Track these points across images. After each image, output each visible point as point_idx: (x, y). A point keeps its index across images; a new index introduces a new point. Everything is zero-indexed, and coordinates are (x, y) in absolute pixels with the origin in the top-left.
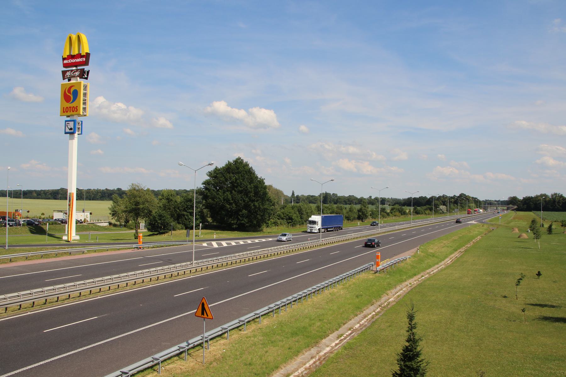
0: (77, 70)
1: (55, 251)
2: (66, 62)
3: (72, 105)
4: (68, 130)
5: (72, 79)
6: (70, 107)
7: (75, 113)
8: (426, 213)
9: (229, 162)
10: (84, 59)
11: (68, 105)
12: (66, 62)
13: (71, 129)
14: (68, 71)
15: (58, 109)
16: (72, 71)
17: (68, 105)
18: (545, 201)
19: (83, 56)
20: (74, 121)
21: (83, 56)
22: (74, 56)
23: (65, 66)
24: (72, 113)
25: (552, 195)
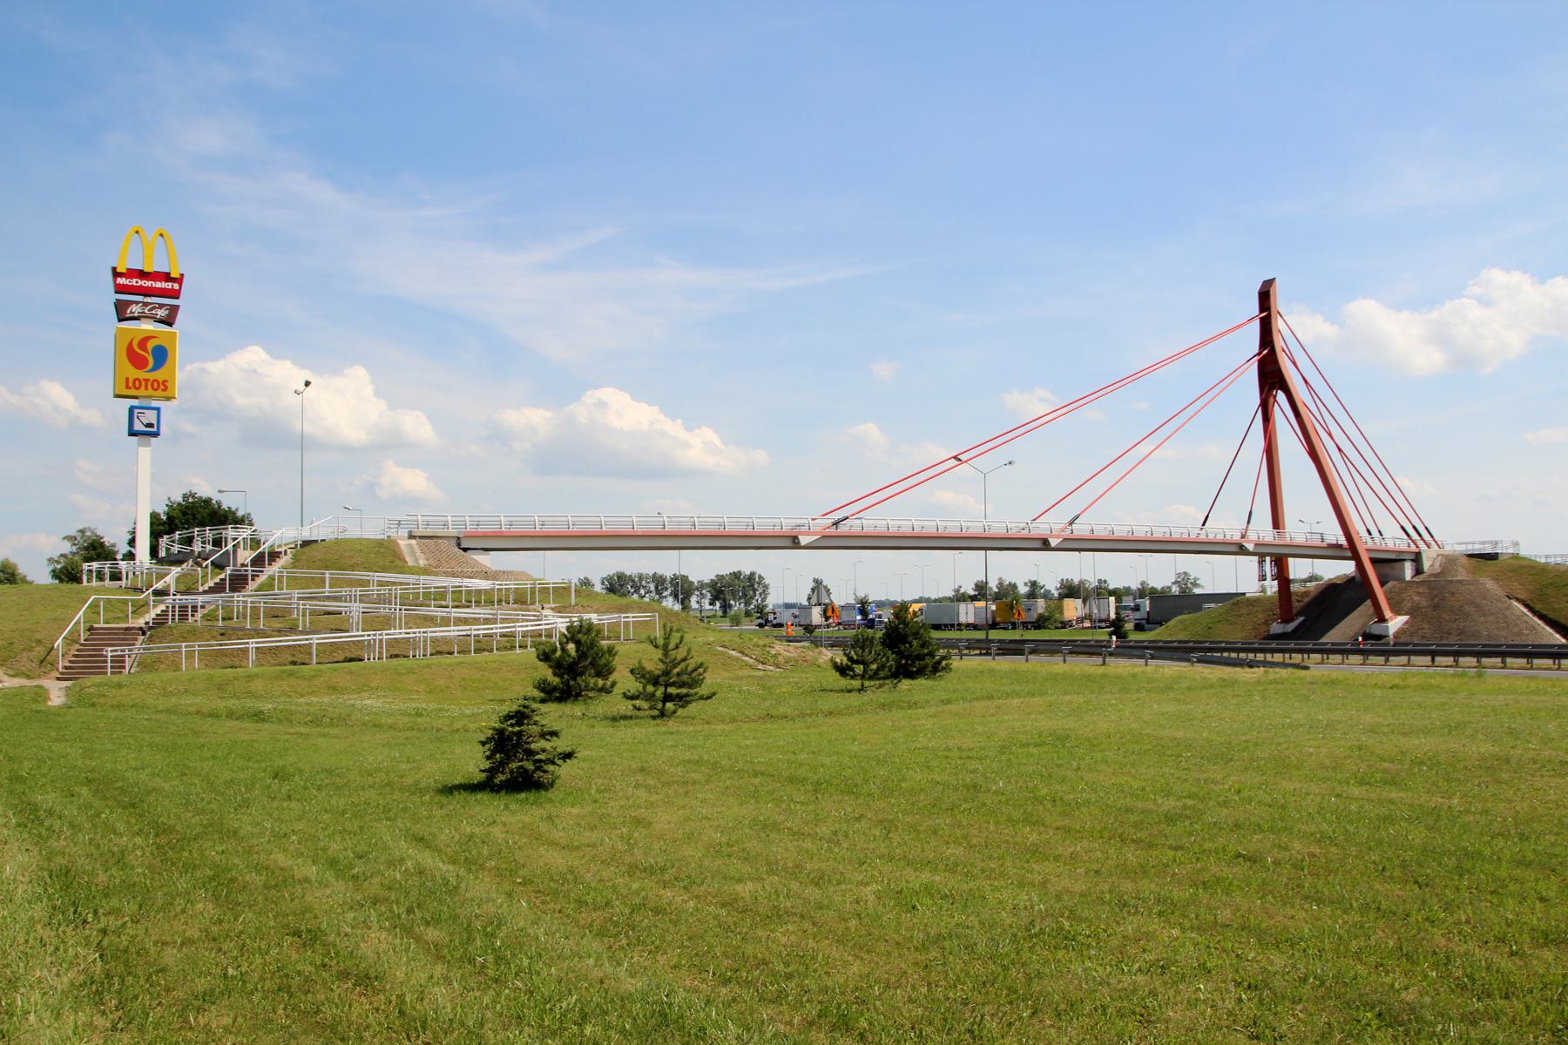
0: (161, 306)
2: (121, 281)
3: (152, 376)
4: (138, 427)
6: (146, 381)
7: (160, 393)
10: (176, 286)
11: (141, 374)
12: (121, 281)
13: (150, 425)
16: (146, 304)
19: (174, 280)
20: (158, 409)
21: (174, 280)
23: (120, 289)
24: (150, 392)
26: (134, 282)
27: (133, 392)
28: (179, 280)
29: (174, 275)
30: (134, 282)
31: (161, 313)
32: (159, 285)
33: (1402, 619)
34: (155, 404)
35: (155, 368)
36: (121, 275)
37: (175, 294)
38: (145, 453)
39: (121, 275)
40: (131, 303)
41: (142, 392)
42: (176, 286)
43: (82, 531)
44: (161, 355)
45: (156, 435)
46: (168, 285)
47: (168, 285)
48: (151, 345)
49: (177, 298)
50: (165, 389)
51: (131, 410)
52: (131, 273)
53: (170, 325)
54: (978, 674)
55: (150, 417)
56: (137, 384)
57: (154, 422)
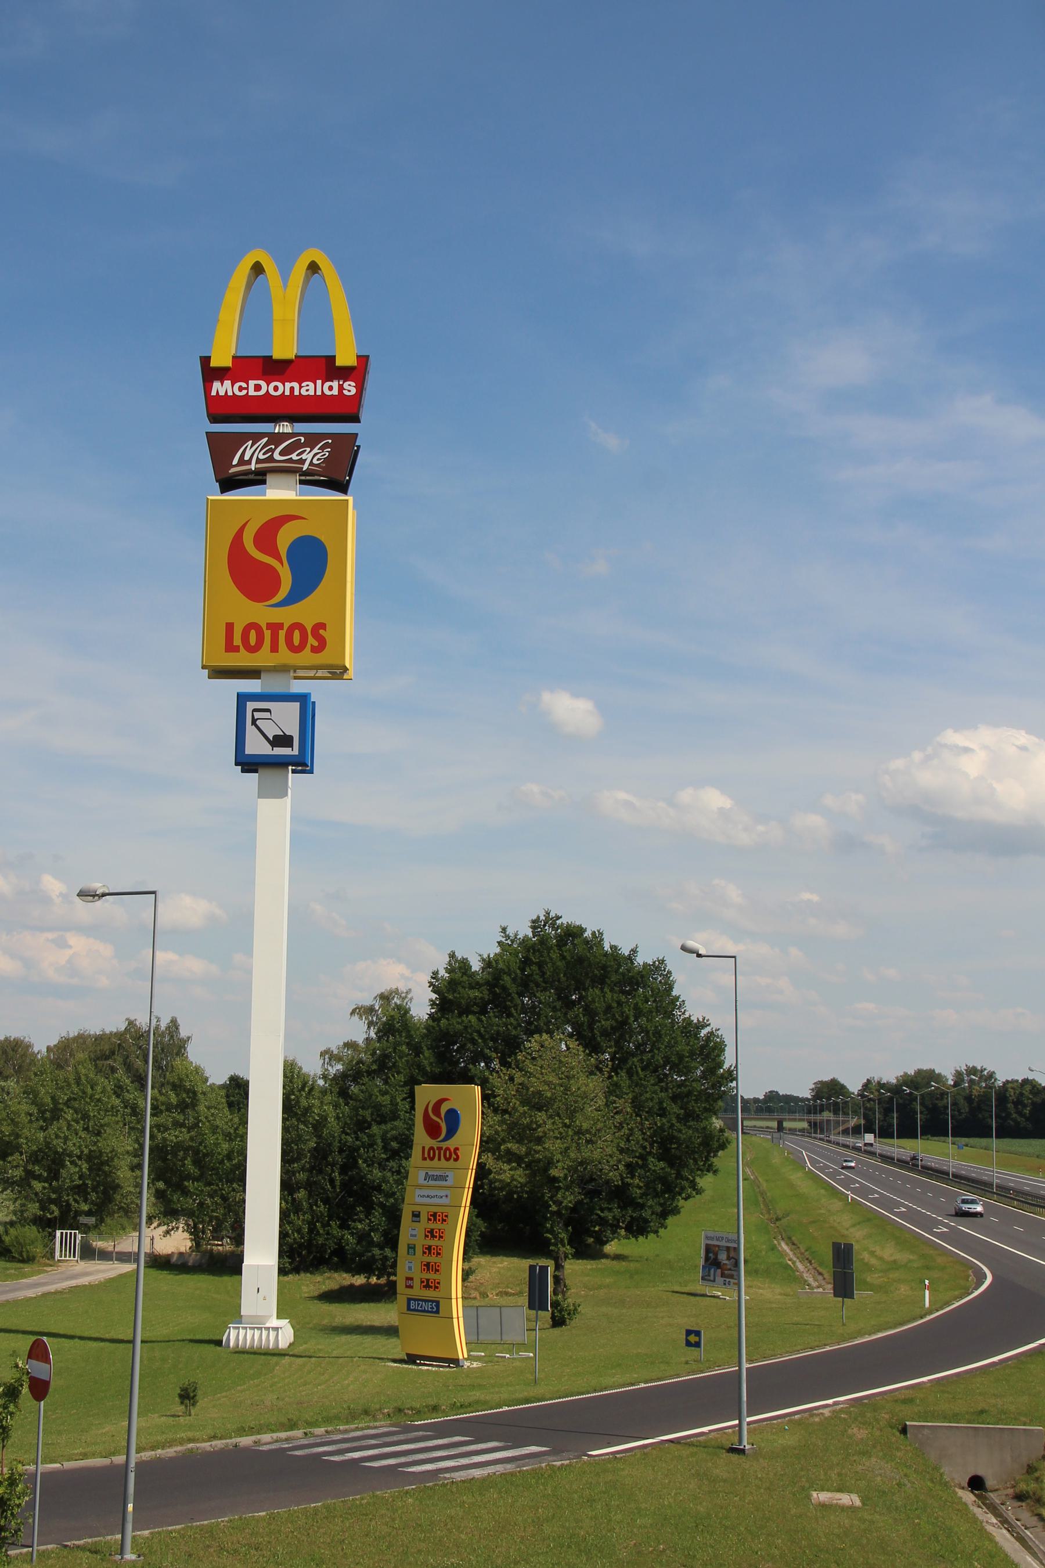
0: (312, 440)
1: (373, 1442)
2: (220, 388)
3: (287, 616)
4: (256, 746)
5: (270, 478)
6: (275, 628)
7: (306, 657)
8: (195, 1396)
9: (131, 1023)
10: (350, 388)
11: (263, 613)
12: (220, 388)
13: (282, 740)
14: (256, 437)
15: (189, 641)
16: (276, 439)
17: (263, 613)
18: (969, 1099)
19: (344, 373)
20: (303, 699)
21: (344, 373)
22: (287, 363)
23: (220, 410)
24: (284, 655)
25: (958, 1075)
26: (255, 388)
27: (243, 659)
28: (357, 372)
29: (345, 358)
30: (255, 388)
31: (311, 457)
32: (309, 389)
33: (133, 1557)
34: (298, 687)
35: (295, 597)
36: (221, 374)
37: (348, 411)
38: (275, 816)
39: (221, 374)
40: (241, 439)
41: (263, 658)
42: (350, 388)
43: (385, 998)
44: (312, 561)
45: (302, 764)
46: (331, 388)
47: (331, 388)
48: (285, 539)
49: (356, 419)
50: (321, 646)
51: (242, 699)
52: (244, 367)
53: (342, 487)
54: (1003, 1535)
55: (285, 718)
56: (252, 637)
57: (293, 729)
